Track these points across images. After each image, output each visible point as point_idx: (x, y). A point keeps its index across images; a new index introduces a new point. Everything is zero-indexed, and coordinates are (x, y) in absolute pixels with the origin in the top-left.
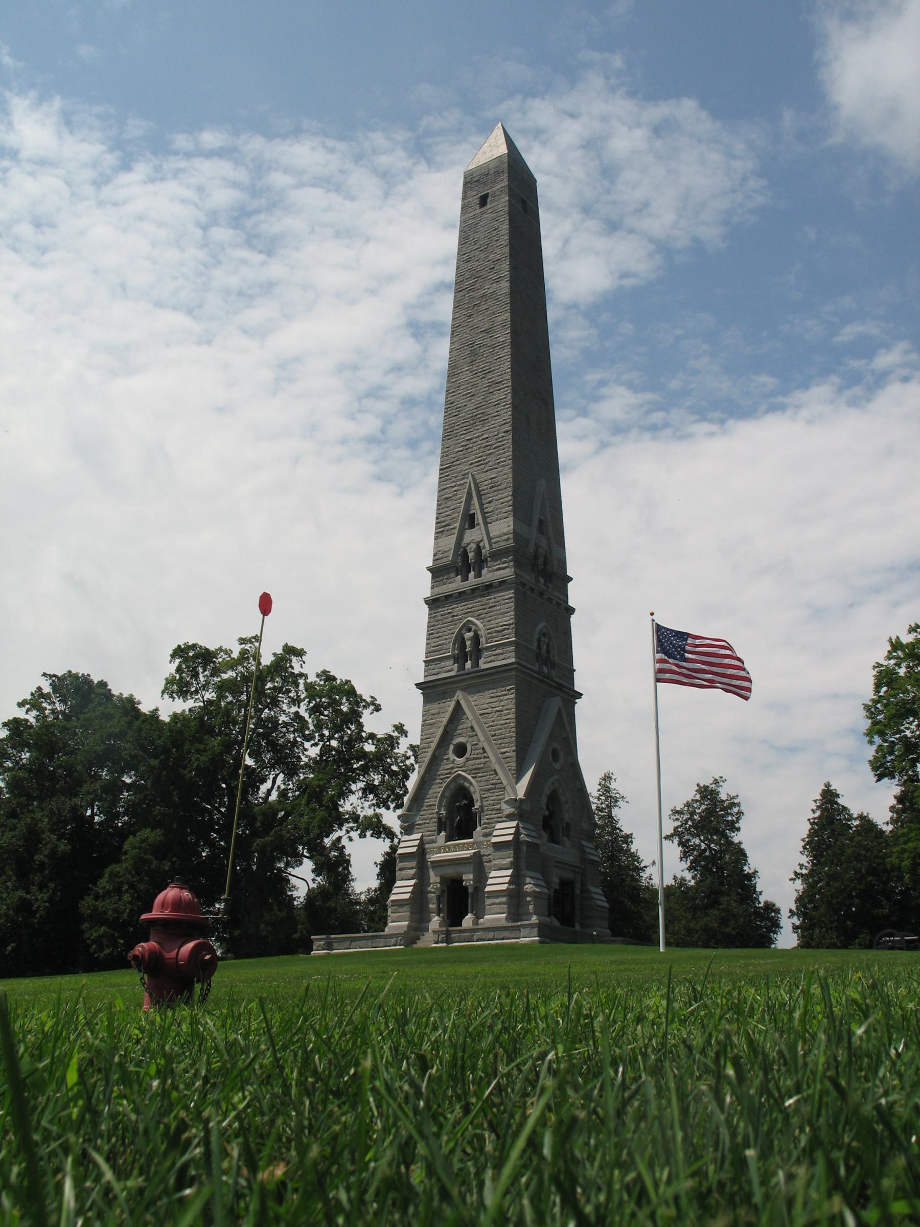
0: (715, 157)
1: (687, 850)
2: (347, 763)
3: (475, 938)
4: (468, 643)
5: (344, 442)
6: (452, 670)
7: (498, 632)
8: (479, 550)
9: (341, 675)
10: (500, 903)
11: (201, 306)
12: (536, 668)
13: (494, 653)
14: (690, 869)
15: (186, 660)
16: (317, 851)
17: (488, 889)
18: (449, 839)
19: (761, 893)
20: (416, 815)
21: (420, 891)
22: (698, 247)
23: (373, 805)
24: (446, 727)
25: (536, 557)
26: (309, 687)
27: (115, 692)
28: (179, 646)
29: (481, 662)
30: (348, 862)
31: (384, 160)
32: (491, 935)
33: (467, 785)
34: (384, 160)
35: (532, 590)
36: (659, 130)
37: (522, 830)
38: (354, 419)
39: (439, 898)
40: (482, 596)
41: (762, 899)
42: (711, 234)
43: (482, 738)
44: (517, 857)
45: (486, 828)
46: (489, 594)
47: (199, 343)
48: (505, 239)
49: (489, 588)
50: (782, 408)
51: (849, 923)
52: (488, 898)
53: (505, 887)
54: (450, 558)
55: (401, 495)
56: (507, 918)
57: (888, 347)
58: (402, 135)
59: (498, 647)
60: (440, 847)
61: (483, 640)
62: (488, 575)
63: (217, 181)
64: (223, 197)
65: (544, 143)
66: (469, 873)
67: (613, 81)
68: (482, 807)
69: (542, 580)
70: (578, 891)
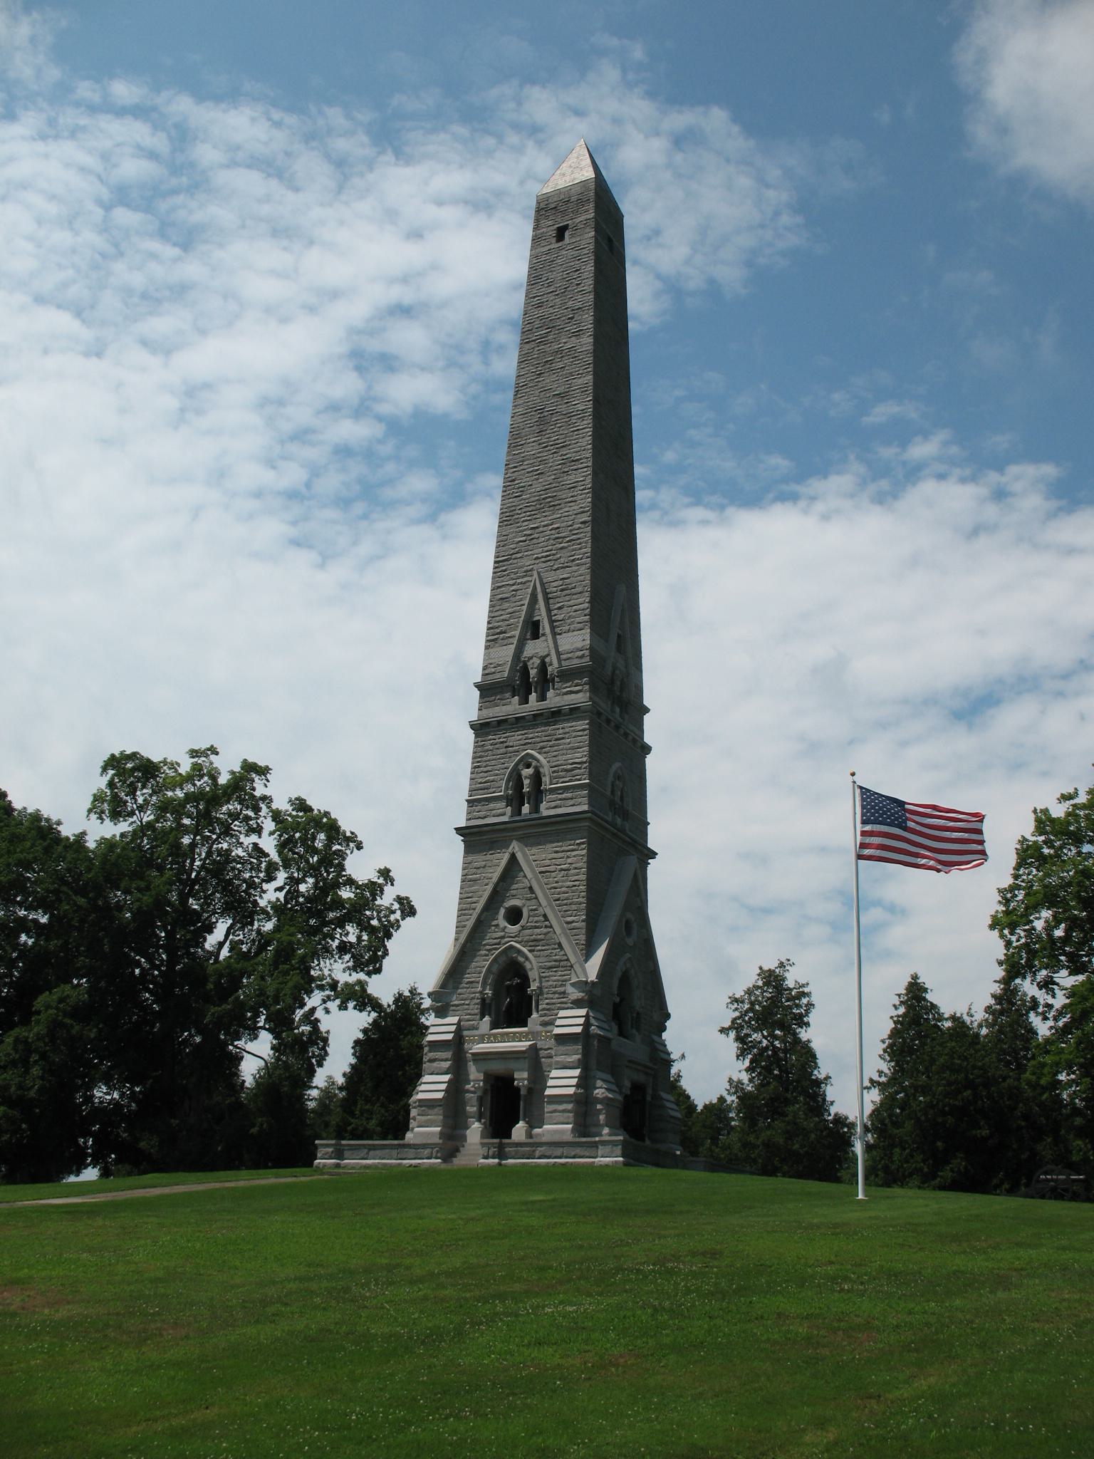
0: (744, 182)
1: (745, 1045)
2: (320, 915)
3: (537, 1154)
4: (526, 782)
5: (258, 494)
8: (543, 667)
9: (317, 804)
10: (564, 1111)
11: (92, 307)
12: (610, 819)
14: (747, 1070)
15: (121, 772)
16: (280, 1024)
17: (548, 1092)
18: (495, 1025)
19: (832, 1103)
20: (451, 994)
21: (455, 1090)
22: (713, 290)
23: (349, 968)
24: (497, 885)
25: (613, 682)
26: (277, 816)
27: (17, 805)
28: (113, 755)
29: (543, 806)
30: (325, 1040)
31: (341, 145)
32: (559, 1151)
33: (521, 959)
34: (341, 145)
35: (608, 721)
36: (680, 141)
37: (592, 1021)
38: (274, 468)
39: (481, 1099)
41: (833, 1110)
42: (730, 275)
43: (544, 902)
44: (586, 1053)
45: (545, 1015)
46: (555, 723)
47: (86, 355)
48: (588, 285)
49: (556, 715)
50: (793, 498)
51: (939, 1144)
52: (549, 1103)
53: (571, 1091)
55: (322, 566)
56: (573, 1130)
57: (926, 435)
58: (365, 116)
59: (566, 789)
60: (483, 1036)
61: (546, 780)
62: (554, 699)
63: (126, 146)
64: (132, 169)
65: (540, 144)
66: (522, 1070)
67: (631, 76)
68: (540, 988)
69: (618, 710)
70: (649, 1098)
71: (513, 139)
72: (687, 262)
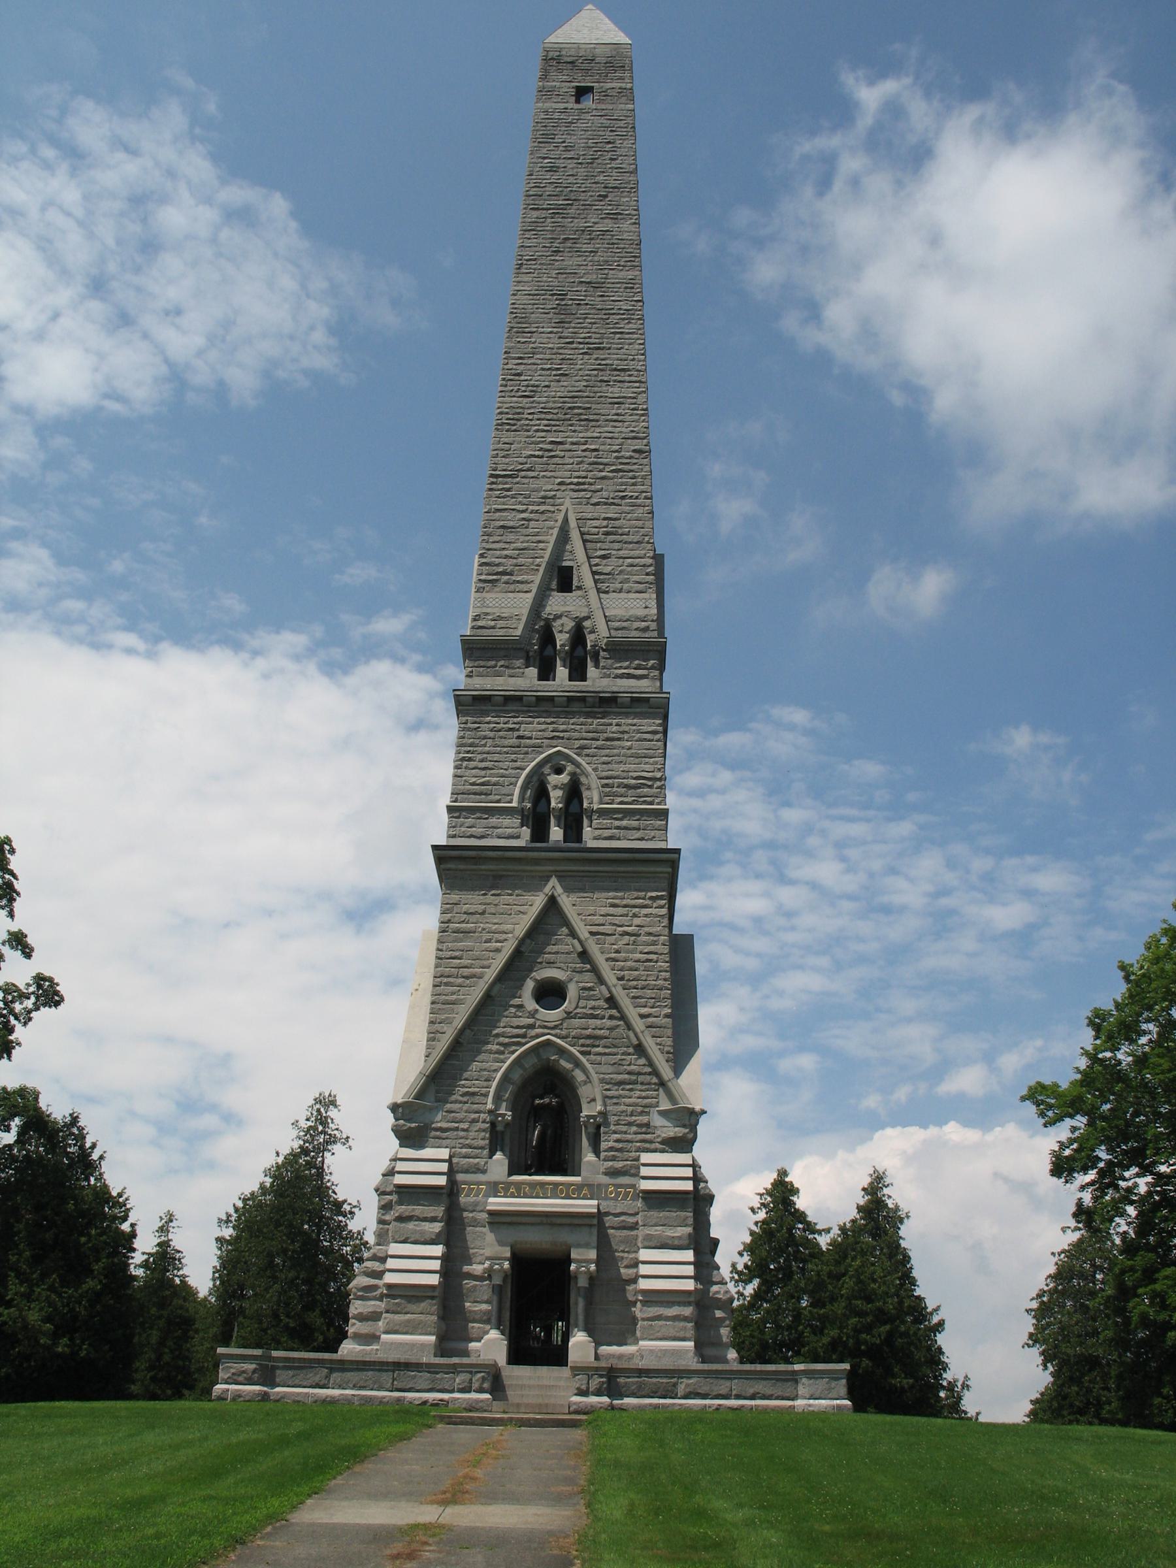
0: (288, 283)
3: (681, 1389)
6: (518, 837)
7: (627, 786)
8: (578, 636)
10: (675, 1318)
13: (617, 823)
20: (436, 1109)
24: (522, 942)
33: (565, 1064)
40: (588, 715)
42: (243, 381)
45: (614, 1159)
50: (237, 646)
54: (519, 632)
60: (496, 1184)
65: (74, 172)
66: (587, 1246)
71: (49, 153)
72: (200, 353)
